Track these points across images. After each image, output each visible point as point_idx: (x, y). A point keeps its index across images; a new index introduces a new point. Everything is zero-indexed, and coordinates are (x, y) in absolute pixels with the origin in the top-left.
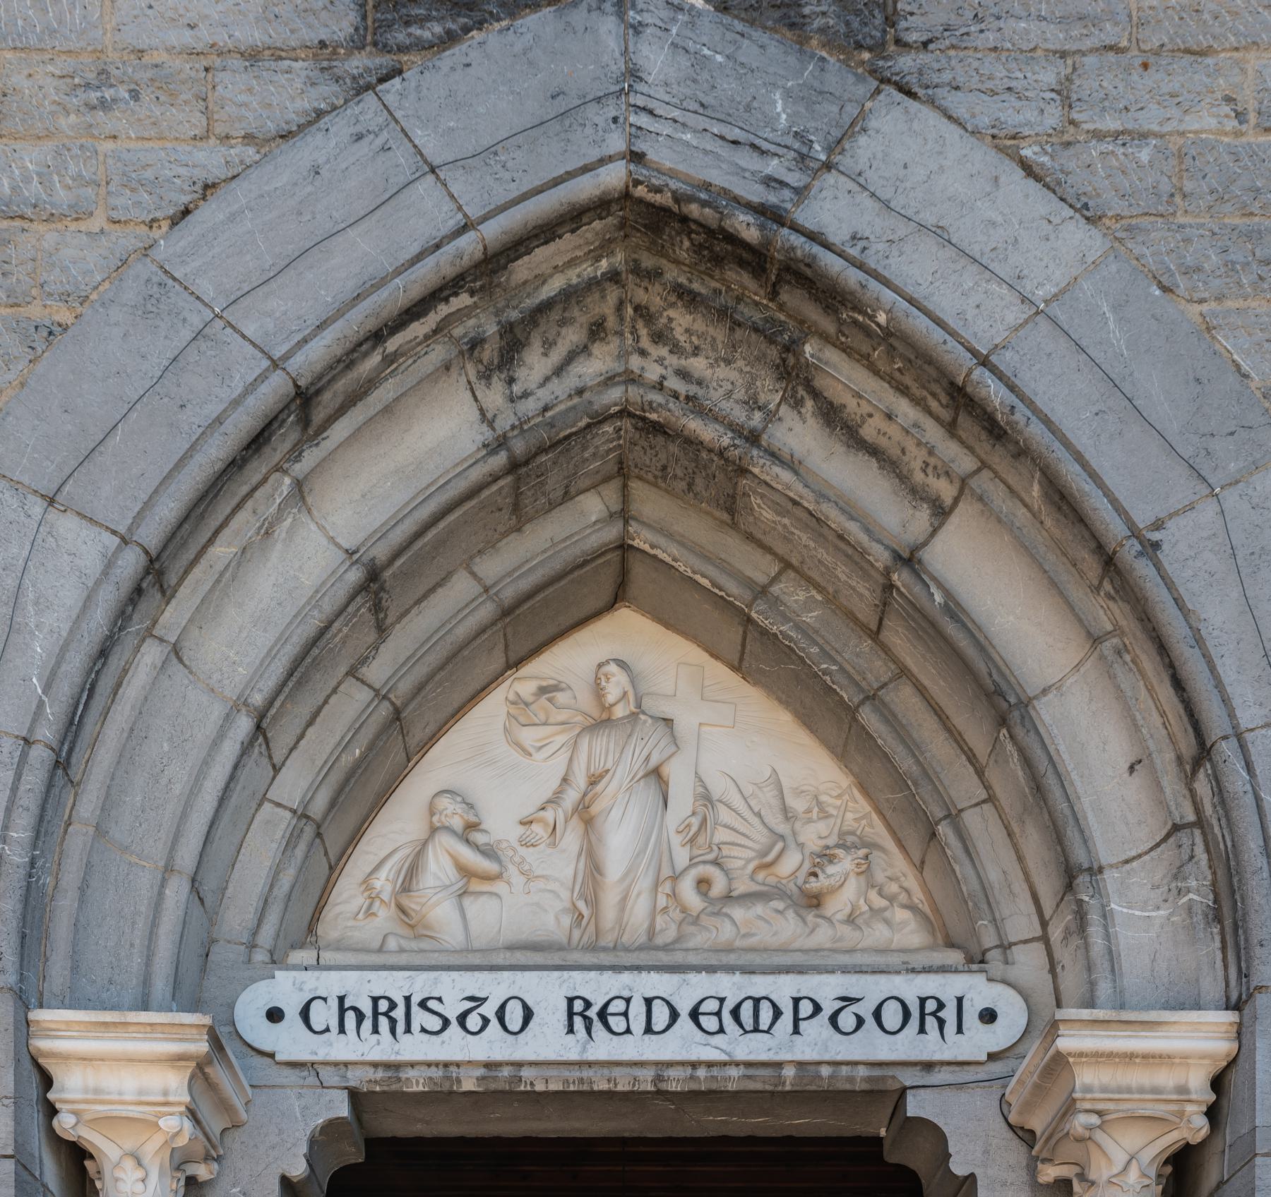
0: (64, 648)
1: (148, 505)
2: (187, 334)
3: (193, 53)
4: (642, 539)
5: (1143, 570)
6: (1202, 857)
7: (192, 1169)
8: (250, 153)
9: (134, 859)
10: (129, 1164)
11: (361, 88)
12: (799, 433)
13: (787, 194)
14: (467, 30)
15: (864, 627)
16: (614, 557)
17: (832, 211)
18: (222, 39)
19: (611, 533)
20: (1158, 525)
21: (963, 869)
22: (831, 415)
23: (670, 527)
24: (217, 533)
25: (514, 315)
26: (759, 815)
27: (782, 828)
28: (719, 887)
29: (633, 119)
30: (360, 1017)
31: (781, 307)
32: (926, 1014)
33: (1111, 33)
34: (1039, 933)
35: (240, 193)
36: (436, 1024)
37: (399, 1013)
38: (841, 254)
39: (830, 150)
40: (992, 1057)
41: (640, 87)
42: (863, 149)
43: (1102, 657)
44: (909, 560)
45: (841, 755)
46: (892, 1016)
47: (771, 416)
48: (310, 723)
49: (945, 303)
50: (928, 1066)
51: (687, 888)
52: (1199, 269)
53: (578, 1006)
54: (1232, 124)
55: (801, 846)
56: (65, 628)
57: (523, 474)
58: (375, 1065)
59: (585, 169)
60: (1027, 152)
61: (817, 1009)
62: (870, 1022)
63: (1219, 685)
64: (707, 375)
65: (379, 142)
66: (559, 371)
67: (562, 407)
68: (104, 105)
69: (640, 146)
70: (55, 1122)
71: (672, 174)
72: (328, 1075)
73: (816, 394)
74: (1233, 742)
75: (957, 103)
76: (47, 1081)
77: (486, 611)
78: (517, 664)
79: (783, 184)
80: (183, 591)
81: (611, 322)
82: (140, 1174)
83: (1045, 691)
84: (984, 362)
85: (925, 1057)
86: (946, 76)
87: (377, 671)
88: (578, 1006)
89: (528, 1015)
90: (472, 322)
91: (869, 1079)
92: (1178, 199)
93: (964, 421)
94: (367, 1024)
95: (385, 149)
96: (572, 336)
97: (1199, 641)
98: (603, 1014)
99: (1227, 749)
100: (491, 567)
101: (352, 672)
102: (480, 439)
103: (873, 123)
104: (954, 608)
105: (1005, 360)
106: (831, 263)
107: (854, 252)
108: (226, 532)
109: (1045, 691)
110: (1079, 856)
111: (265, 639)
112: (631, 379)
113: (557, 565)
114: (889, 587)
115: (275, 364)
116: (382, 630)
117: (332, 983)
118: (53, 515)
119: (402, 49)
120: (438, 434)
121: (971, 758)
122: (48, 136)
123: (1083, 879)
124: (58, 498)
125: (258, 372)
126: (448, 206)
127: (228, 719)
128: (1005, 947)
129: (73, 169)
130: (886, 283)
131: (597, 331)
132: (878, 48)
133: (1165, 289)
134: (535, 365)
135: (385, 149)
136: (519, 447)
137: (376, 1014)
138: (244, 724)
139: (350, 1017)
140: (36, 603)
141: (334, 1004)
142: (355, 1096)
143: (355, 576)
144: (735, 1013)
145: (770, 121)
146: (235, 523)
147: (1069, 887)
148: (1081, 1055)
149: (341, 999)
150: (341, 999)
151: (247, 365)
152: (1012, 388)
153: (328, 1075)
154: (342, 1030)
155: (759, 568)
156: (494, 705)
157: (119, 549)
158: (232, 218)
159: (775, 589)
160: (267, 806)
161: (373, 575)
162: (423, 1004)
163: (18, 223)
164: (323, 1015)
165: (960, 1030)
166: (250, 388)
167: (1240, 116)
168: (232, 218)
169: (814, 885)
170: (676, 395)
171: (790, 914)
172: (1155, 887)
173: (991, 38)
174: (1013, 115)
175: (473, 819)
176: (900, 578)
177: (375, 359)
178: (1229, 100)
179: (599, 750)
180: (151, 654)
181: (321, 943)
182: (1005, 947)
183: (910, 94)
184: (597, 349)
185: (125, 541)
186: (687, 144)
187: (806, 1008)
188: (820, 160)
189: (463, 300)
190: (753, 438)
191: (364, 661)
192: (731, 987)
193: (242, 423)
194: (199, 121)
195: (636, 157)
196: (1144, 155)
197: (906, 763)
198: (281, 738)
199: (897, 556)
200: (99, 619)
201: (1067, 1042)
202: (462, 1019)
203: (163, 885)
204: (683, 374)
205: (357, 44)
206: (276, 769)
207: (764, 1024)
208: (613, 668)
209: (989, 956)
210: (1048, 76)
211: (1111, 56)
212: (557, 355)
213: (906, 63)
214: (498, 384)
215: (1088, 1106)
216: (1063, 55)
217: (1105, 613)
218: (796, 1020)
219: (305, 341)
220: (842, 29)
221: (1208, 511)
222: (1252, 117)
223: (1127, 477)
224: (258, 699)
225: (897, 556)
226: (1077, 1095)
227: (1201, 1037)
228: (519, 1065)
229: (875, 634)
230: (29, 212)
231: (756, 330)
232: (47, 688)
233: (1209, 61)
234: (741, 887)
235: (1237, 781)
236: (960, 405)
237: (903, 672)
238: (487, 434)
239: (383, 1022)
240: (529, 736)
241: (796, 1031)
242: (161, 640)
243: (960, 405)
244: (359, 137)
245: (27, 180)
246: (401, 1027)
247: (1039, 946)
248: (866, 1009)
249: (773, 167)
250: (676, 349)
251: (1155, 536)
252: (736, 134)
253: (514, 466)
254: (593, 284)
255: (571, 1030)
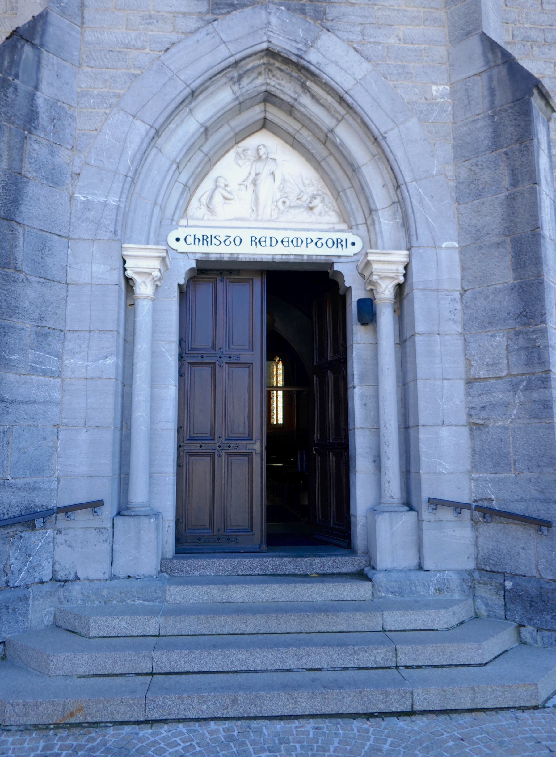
0: (136, 153)
1: (157, 118)
2: (167, 78)
3: (170, 12)
4: (269, 117)
5: (383, 143)
6: (400, 210)
7: (156, 283)
8: (183, 36)
9: (147, 201)
10: (143, 284)
11: (209, 22)
12: (306, 100)
13: (302, 52)
14: (232, 11)
15: (322, 142)
16: (263, 120)
17: (313, 57)
18: (177, 10)
19: (262, 116)
20: (386, 133)
21: (347, 205)
22: (313, 97)
23: (275, 115)
24: (171, 121)
25: (241, 72)
26: (297, 185)
27: (303, 189)
28: (288, 204)
29: (269, 33)
30: (199, 240)
31: (302, 73)
32: (338, 243)
33: (371, 20)
34: (364, 222)
35: (181, 45)
36: (218, 243)
37: (209, 240)
38: (315, 66)
39: (312, 42)
40: (355, 254)
41: (270, 26)
42: (319, 43)
43: (375, 160)
44: (332, 131)
45: (317, 170)
46: (330, 243)
47: (299, 95)
48: (189, 161)
49: (338, 79)
50: (339, 256)
51: (280, 204)
52: (392, 74)
53: (254, 239)
54: (398, 42)
55: (307, 193)
56: (136, 148)
57: (241, 106)
58: (202, 253)
59: (259, 44)
60: (355, 46)
61: (312, 241)
62: (325, 244)
63: (401, 171)
64: (286, 87)
65: (212, 35)
66: (251, 82)
67: (251, 91)
68: (150, 23)
69: (270, 40)
70: (126, 273)
71: (277, 46)
72: (191, 256)
73: (309, 92)
74: (405, 185)
75: (340, 34)
76: (124, 262)
77: (232, 134)
78: (238, 143)
79: (301, 50)
80: (162, 136)
81: (263, 72)
82: (145, 287)
83: (363, 165)
84: (347, 92)
85: (338, 254)
86: (337, 28)
87: (205, 149)
88: (254, 239)
89: (241, 241)
90: (231, 73)
91: (325, 260)
92: (387, 58)
93: (342, 102)
94: (201, 242)
95: (214, 37)
96: (254, 75)
97: (396, 160)
98: (260, 241)
99: (403, 187)
100: (233, 123)
101: (199, 149)
102: (232, 98)
103: (321, 37)
104: (342, 143)
105: (351, 93)
106: (313, 68)
107: (317, 66)
108: (173, 121)
109: (363, 165)
110: (373, 207)
111: (180, 145)
112: (268, 84)
113: (249, 123)
114: (327, 136)
115: (187, 86)
116: (207, 139)
117: (192, 231)
118: (135, 120)
119: (218, 14)
120: (224, 96)
121: (348, 176)
122: (137, 30)
123: (373, 213)
124: (136, 116)
125: (183, 88)
126: (227, 51)
127: (171, 165)
128: (357, 225)
129: (142, 38)
130: (325, 73)
131: (260, 74)
132: (322, 20)
133: (385, 78)
134: (245, 81)
135: (214, 37)
136: (241, 99)
137: (203, 239)
138: (175, 166)
139: (197, 240)
140: (130, 141)
141: (193, 237)
142: (197, 261)
143: (202, 130)
144: (292, 241)
145: (299, 35)
146: (175, 119)
147: (371, 213)
148: (373, 261)
149: (195, 236)
150: (195, 236)
151: (181, 86)
152: (353, 99)
153: (191, 256)
154: (195, 244)
155: (297, 126)
156: (231, 155)
157: (150, 129)
158: (179, 51)
159: (301, 131)
160: (177, 183)
161: (206, 129)
162: (215, 237)
163: (129, 50)
164: (190, 240)
165: (346, 247)
166: (181, 91)
167: (400, 40)
168: (179, 51)
169: (311, 205)
170: (277, 89)
171: (305, 212)
172: (390, 216)
173: (346, 20)
174: (351, 37)
175: (226, 184)
176: (330, 135)
177: (210, 82)
178: (397, 36)
179: (259, 167)
180: (154, 151)
181: (188, 216)
182: (357, 225)
183: (328, 30)
184: (260, 77)
185: (151, 127)
186: (281, 40)
187: (309, 241)
188: (311, 43)
189: (230, 69)
190: (296, 100)
191: (202, 146)
192: (292, 235)
193: (179, 99)
194: (172, 28)
195: (269, 42)
196: (380, 48)
197: (333, 177)
198: (181, 168)
199: (329, 130)
200: (145, 145)
201: (370, 258)
202: (225, 242)
203: (154, 207)
204: (279, 84)
205: (207, 12)
206: (180, 173)
207: (299, 245)
208: (261, 147)
209: (353, 227)
210: (359, 29)
211: (372, 25)
212: (250, 79)
213: (328, 24)
214: (237, 85)
215: (376, 273)
216: (362, 24)
217: (374, 149)
218: (307, 244)
219: (194, 81)
220: (314, 15)
221: (396, 131)
222: (402, 40)
223: (379, 121)
224: (178, 160)
225: (329, 130)
226: (373, 271)
227: (401, 256)
228: (239, 254)
229: (324, 144)
230: (132, 47)
231: (296, 78)
232: (132, 162)
233: (393, 27)
234: (292, 205)
235: (406, 194)
236: (341, 100)
237: (331, 153)
238: (234, 96)
239: (205, 242)
240: (240, 162)
241: (307, 247)
242: (157, 148)
243: (341, 100)
244: (208, 34)
245: (132, 40)
246: (209, 243)
247: (365, 225)
248: (324, 241)
249: (300, 46)
250: (278, 79)
251: (385, 135)
252: (291, 38)
253: (240, 103)
254: (259, 66)
255: (252, 245)
